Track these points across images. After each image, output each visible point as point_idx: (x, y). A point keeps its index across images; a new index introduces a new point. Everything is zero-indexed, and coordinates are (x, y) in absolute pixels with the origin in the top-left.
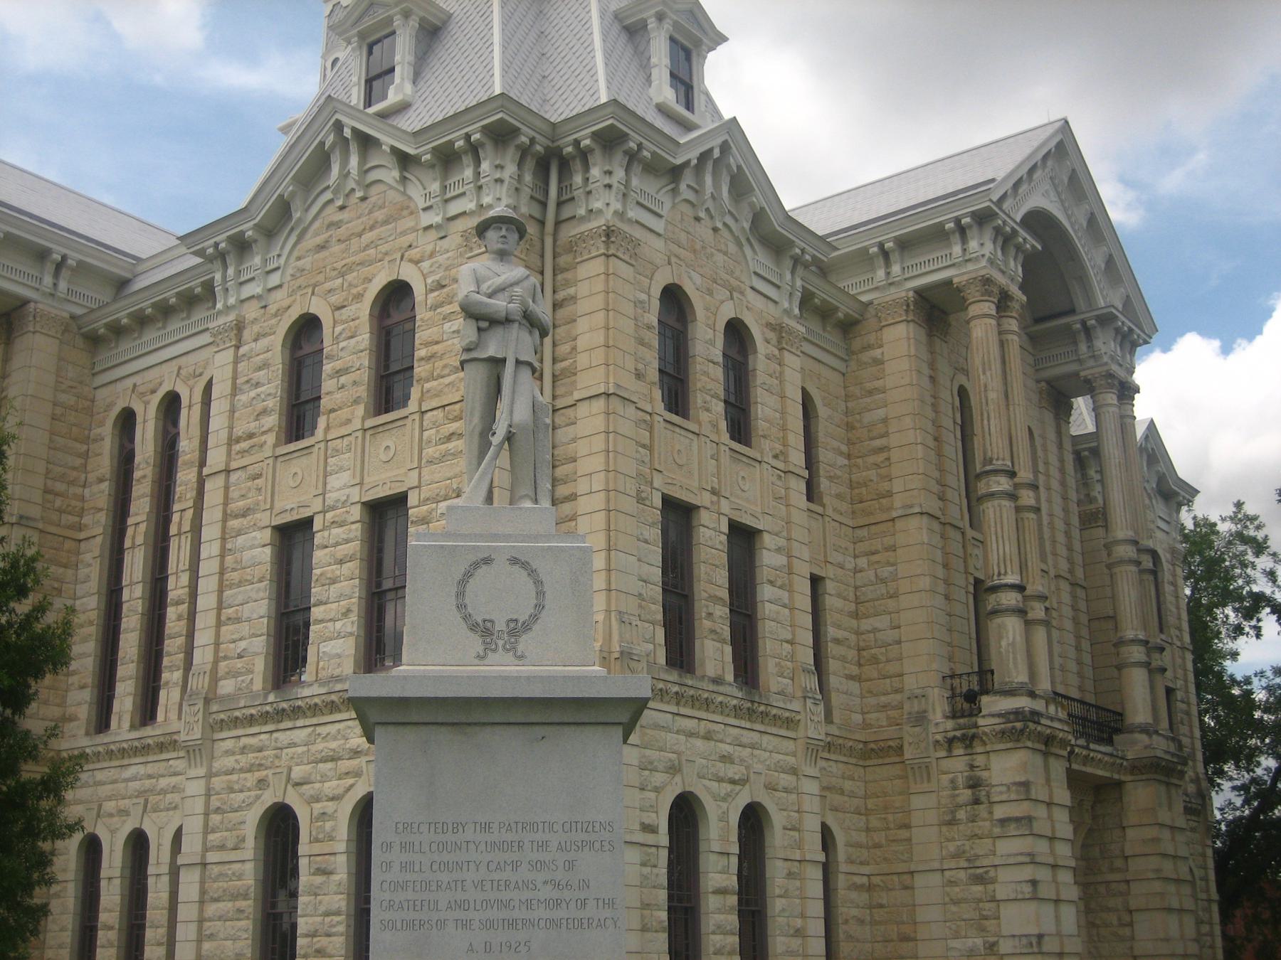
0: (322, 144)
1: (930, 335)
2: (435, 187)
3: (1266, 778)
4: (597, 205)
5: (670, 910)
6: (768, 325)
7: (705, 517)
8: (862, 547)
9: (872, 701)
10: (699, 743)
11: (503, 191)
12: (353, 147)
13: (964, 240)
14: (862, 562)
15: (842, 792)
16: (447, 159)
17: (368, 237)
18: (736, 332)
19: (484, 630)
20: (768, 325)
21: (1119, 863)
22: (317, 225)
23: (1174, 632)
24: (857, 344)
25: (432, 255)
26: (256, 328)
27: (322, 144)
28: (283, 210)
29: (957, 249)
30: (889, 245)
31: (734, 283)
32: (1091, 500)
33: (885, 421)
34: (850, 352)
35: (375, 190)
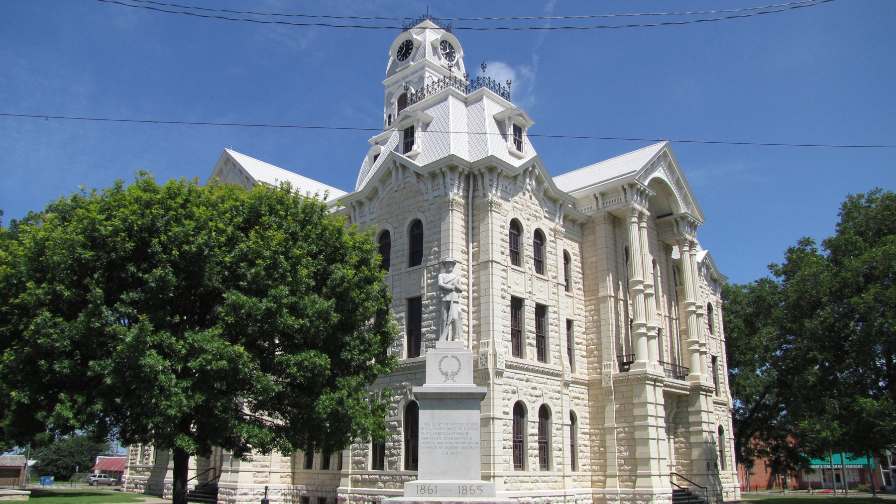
1: (614, 227)
5: (514, 441)
6: (551, 229)
7: (527, 302)
10: (524, 383)
12: (400, 169)
15: (579, 398)
18: (539, 235)
20: (551, 229)
23: (717, 334)
25: (429, 209)
28: (375, 191)
31: (538, 215)
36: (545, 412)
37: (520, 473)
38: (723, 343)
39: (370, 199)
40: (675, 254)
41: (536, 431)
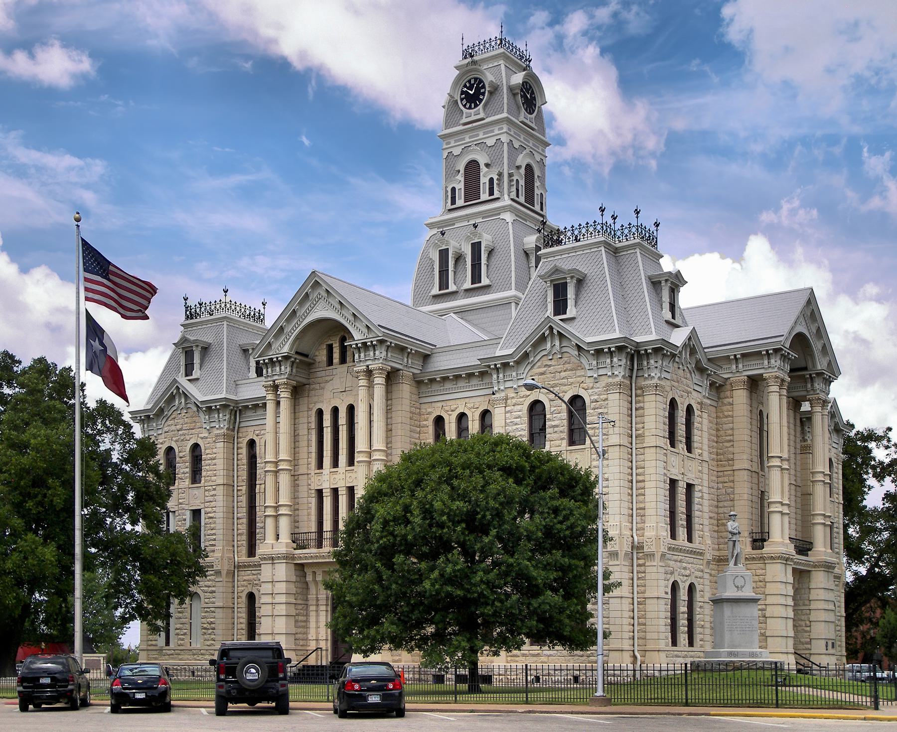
0: (544, 333)
2: (595, 363)
3: (887, 505)
4: (653, 374)
6: (698, 403)
8: (720, 479)
9: (721, 540)
11: (621, 370)
13: (769, 359)
14: (720, 485)
16: (599, 353)
17: (563, 374)
19: (737, 587)
21: (807, 602)
22: (539, 364)
24: (722, 395)
26: (514, 401)
27: (544, 333)
29: (766, 362)
30: (738, 356)
32: (805, 440)
33: (732, 429)
34: (719, 398)
35: (566, 355)
36: (691, 589)
37: (674, 648)
38: (841, 507)
39: (518, 363)
40: (806, 407)
41: (685, 609)
